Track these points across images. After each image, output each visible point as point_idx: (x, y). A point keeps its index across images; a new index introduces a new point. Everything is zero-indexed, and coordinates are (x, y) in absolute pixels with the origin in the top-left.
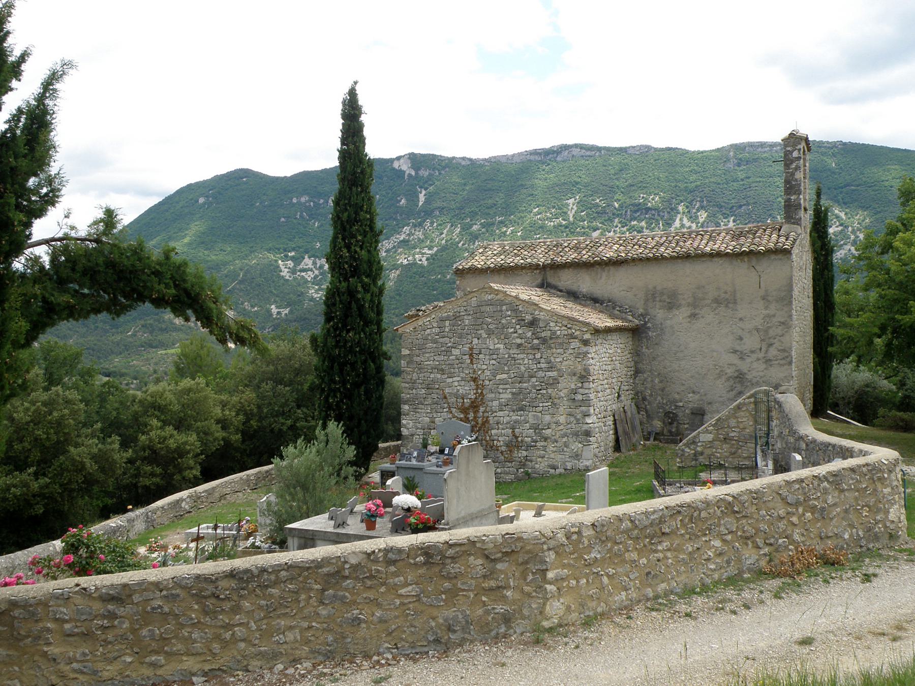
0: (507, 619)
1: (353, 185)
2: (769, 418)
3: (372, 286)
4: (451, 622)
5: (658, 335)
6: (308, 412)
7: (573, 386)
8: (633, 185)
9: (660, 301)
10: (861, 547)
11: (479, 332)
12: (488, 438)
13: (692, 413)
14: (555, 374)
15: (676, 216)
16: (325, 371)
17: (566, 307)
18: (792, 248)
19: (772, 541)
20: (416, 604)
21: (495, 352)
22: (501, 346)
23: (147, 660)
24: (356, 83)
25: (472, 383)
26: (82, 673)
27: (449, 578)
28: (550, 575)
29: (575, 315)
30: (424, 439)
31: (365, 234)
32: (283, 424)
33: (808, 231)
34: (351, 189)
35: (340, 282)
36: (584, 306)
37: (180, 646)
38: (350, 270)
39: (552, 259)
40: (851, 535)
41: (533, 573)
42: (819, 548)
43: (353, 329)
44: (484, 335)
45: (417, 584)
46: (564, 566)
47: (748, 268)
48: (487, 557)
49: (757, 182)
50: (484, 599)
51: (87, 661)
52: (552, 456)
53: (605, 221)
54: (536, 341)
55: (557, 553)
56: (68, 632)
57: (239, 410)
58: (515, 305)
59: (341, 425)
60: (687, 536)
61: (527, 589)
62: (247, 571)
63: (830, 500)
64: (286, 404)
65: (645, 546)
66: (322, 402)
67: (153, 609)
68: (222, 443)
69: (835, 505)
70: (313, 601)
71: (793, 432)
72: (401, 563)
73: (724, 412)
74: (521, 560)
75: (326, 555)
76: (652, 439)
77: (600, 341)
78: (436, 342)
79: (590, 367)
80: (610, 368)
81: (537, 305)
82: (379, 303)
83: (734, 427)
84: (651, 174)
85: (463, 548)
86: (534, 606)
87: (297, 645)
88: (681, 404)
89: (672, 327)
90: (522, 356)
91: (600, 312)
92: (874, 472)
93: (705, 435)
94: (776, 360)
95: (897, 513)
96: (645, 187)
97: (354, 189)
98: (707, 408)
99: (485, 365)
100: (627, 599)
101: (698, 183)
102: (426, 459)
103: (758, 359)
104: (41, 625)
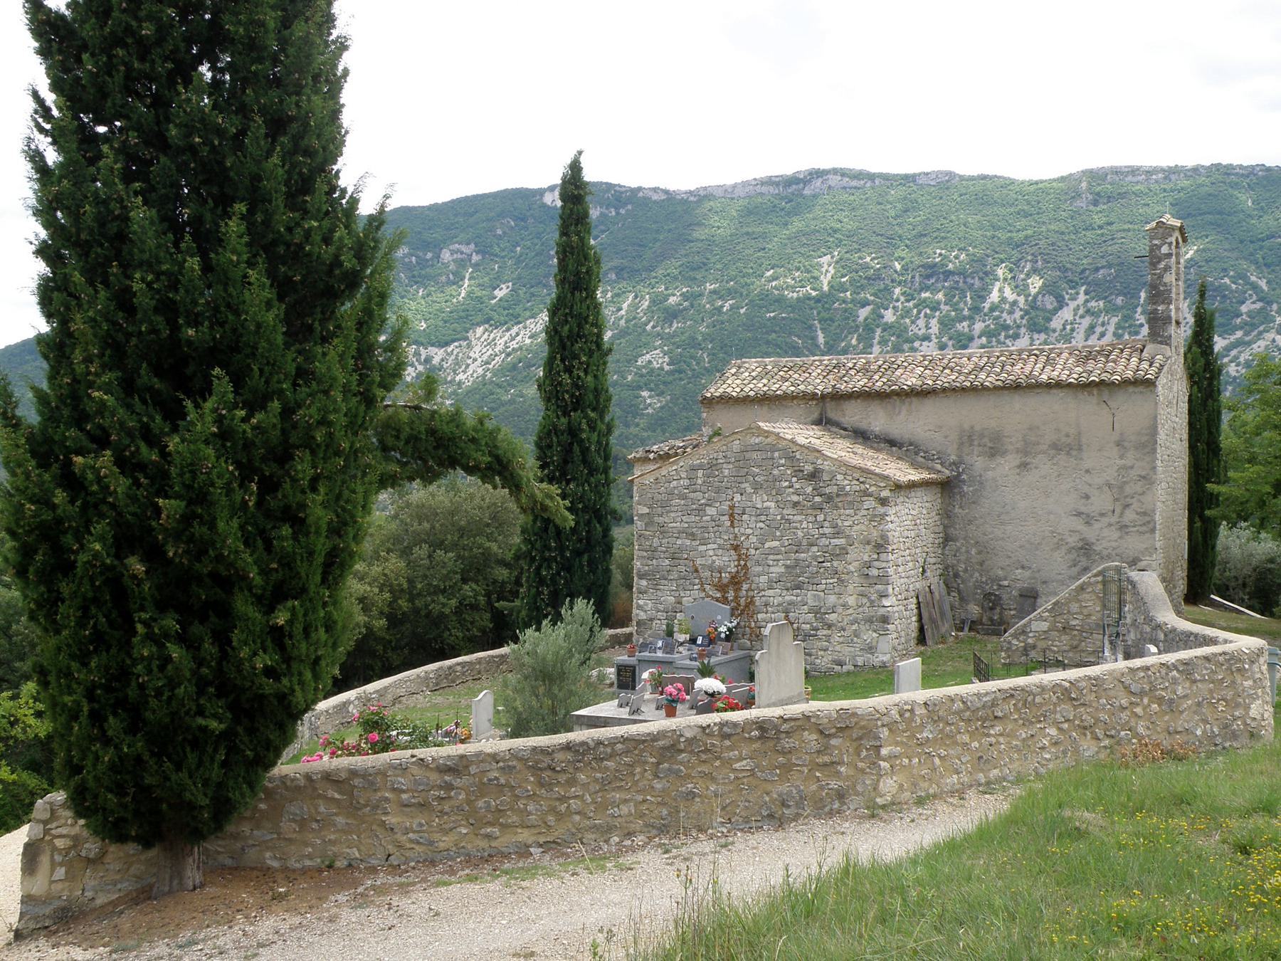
0: (841, 795)
1: (575, 289)
2: (1121, 603)
3: (599, 422)
4: (785, 797)
5: (976, 490)
6: (478, 589)
7: (866, 558)
8: (925, 235)
9: (980, 445)
10: (1216, 745)
11: (743, 486)
12: (753, 624)
13: (1021, 595)
14: (842, 541)
15: (993, 285)
16: (535, 534)
17: (855, 453)
18: (1157, 378)
19: (1113, 732)
20: (751, 778)
21: (763, 512)
22: (772, 505)
23: (483, 831)
24: (580, 153)
25: (733, 552)
26: (418, 843)
27: (783, 753)
28: (884, 751)
29: (869, 464)
30: (668, 625)
31: (590, 355)
32: (444, 605)
33: (1182, 351)
34: (573, 294)
35: (558, 417)
36: (878, 450)
37: (515, 818)
38: (572, 402)
39: (834, 386)
40: (1204, 732)
41: (867, 749)
42: (1166, 744)
43: (574, 479)
44: (749, 490)
45: (751, 758)
46: (897, 744)
47: (1098, 404)
48: (821, 732)
49: (1124, 230)
50: (818, 774)
51: (423, 831)
52: (838, 648)
53: (880, 291)
54: (818, 499)
55: (890, 730)
56: (406, 802)
57: (383, 585)
58: (790, 452)
59: (591, 603)
60: (1021, 722)
61: (861, 765)
62: (583, 743)
63: (1180, 691)
64: (446, 578)
65: (977, 729)
66: (532, 575)
67: (490, 780)
68: (364, 630)
69: (1186, 696)
70: (648, 775)
71: (1149, 620)
72: (735, 737)
73: (1064, 594)
74: (855, 736)
75: (661, 729)
76: (966, 629)
77: (901, 499)
78: (684, 497)
79: (889, 534)
80: (913, 534)
81: (819, 451)
82: (607, 444)
83: (1075, 613)
84: (953, 218)
85: (798, 723)
86: (868, 782)
87: (631, 818)
88: (1006, 583)
89: (994, 479)
90: (799, 518)
91: (899, 458)
92: (1233, 662)
93: (1038, 623)
94: (1134, 526)
95: (1260, 710)
96: (943, 238)
97: (577, 294)
98: (1040, 588)
99: (749, 530)
100: (959, 783)
101: (1030, 232)
102: (676, 650)
103: (1110, 525)
104: (379, 794)
